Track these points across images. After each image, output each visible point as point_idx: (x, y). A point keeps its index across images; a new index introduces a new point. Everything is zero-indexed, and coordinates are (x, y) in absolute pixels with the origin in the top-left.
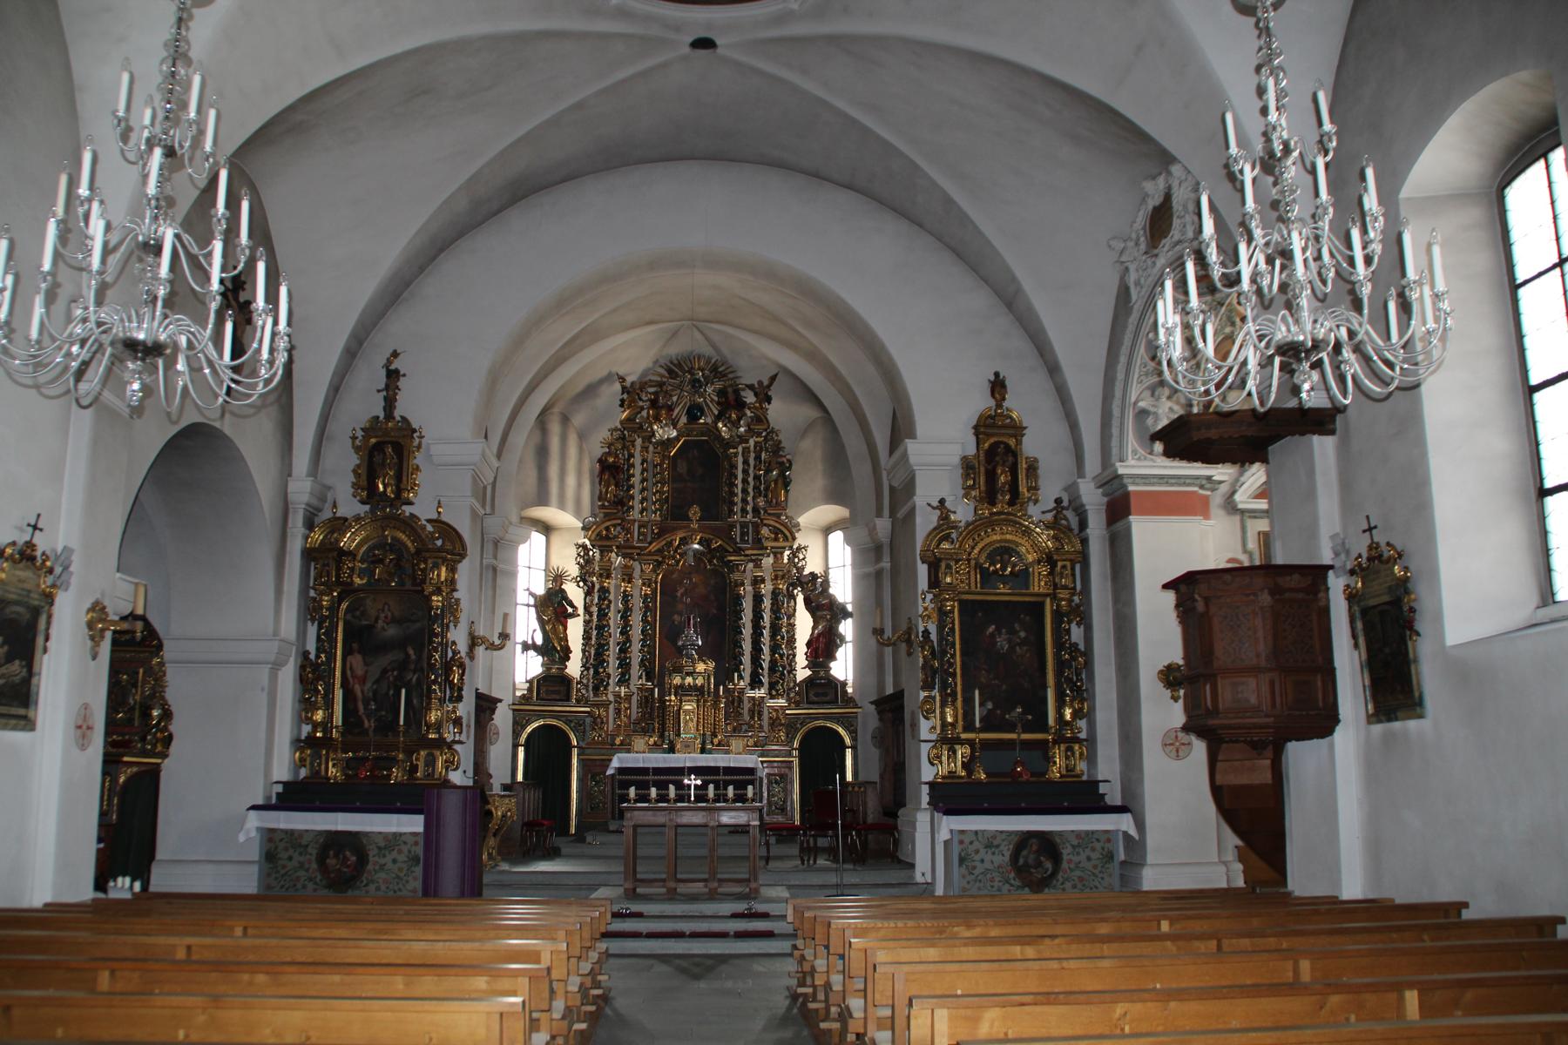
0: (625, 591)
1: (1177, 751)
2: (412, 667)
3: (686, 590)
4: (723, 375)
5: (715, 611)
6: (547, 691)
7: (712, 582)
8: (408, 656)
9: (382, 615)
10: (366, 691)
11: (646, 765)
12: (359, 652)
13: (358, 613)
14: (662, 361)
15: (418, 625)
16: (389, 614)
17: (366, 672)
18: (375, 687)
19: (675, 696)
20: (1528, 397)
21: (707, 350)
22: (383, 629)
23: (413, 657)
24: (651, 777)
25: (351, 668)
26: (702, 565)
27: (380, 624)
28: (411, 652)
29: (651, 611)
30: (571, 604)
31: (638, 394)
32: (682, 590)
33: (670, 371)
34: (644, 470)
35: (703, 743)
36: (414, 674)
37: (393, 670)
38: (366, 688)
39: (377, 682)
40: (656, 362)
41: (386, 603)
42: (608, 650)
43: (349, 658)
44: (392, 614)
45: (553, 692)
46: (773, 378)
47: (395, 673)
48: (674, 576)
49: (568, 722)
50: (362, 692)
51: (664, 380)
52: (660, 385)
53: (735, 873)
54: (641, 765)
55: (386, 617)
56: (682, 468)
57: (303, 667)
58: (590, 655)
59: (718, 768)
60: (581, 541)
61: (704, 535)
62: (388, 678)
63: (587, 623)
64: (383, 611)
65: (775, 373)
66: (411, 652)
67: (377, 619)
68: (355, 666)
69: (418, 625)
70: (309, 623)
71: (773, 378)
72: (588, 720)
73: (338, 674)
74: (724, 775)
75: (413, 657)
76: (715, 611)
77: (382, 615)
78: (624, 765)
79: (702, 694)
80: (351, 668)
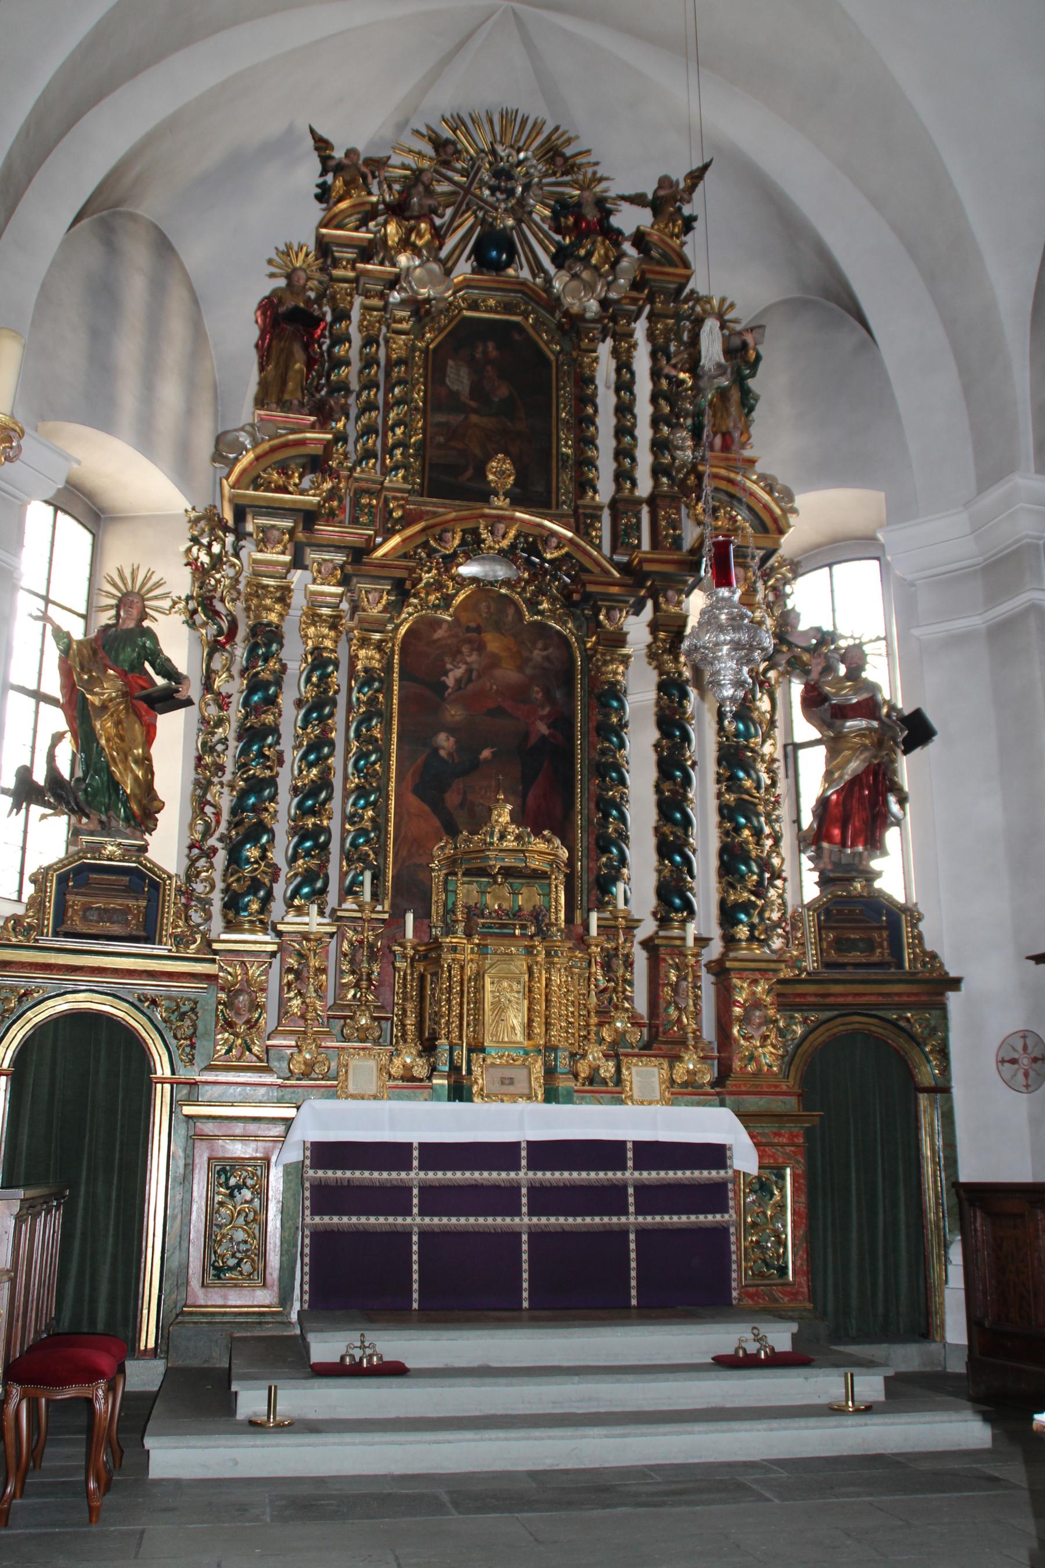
0: (317, 650)
1: (1013, 1061)
3: (469, 671)
4: (570, 167)
5: (543, 729)
6: (87, 908)
7: (537, 654)
19: (469, 935)
21: (534, 109)
24: (415, 1176)
26: (511, 611)
29: (379, 714)
30: (167, 670)
31: (364, 177)
32: (459, 672)
33: (439, 144)
34: (370, 384)
35: (550, 1072)
40: (401, 127)
42: (273, 799)
45: (106, 914)
46: (696, 177)
48: (440, 633)
49: (145, 1004)
51: (426, 164)
53: (222, 1104)
58: (218, 815)
59: (619, 1146)
60: (268, 272)
63: (208, 726)
65: (697, 164)
71: (696, 177)
72: (211, 998)
73: (854, 1188)
76: (543, 729)
79: (543, 933)
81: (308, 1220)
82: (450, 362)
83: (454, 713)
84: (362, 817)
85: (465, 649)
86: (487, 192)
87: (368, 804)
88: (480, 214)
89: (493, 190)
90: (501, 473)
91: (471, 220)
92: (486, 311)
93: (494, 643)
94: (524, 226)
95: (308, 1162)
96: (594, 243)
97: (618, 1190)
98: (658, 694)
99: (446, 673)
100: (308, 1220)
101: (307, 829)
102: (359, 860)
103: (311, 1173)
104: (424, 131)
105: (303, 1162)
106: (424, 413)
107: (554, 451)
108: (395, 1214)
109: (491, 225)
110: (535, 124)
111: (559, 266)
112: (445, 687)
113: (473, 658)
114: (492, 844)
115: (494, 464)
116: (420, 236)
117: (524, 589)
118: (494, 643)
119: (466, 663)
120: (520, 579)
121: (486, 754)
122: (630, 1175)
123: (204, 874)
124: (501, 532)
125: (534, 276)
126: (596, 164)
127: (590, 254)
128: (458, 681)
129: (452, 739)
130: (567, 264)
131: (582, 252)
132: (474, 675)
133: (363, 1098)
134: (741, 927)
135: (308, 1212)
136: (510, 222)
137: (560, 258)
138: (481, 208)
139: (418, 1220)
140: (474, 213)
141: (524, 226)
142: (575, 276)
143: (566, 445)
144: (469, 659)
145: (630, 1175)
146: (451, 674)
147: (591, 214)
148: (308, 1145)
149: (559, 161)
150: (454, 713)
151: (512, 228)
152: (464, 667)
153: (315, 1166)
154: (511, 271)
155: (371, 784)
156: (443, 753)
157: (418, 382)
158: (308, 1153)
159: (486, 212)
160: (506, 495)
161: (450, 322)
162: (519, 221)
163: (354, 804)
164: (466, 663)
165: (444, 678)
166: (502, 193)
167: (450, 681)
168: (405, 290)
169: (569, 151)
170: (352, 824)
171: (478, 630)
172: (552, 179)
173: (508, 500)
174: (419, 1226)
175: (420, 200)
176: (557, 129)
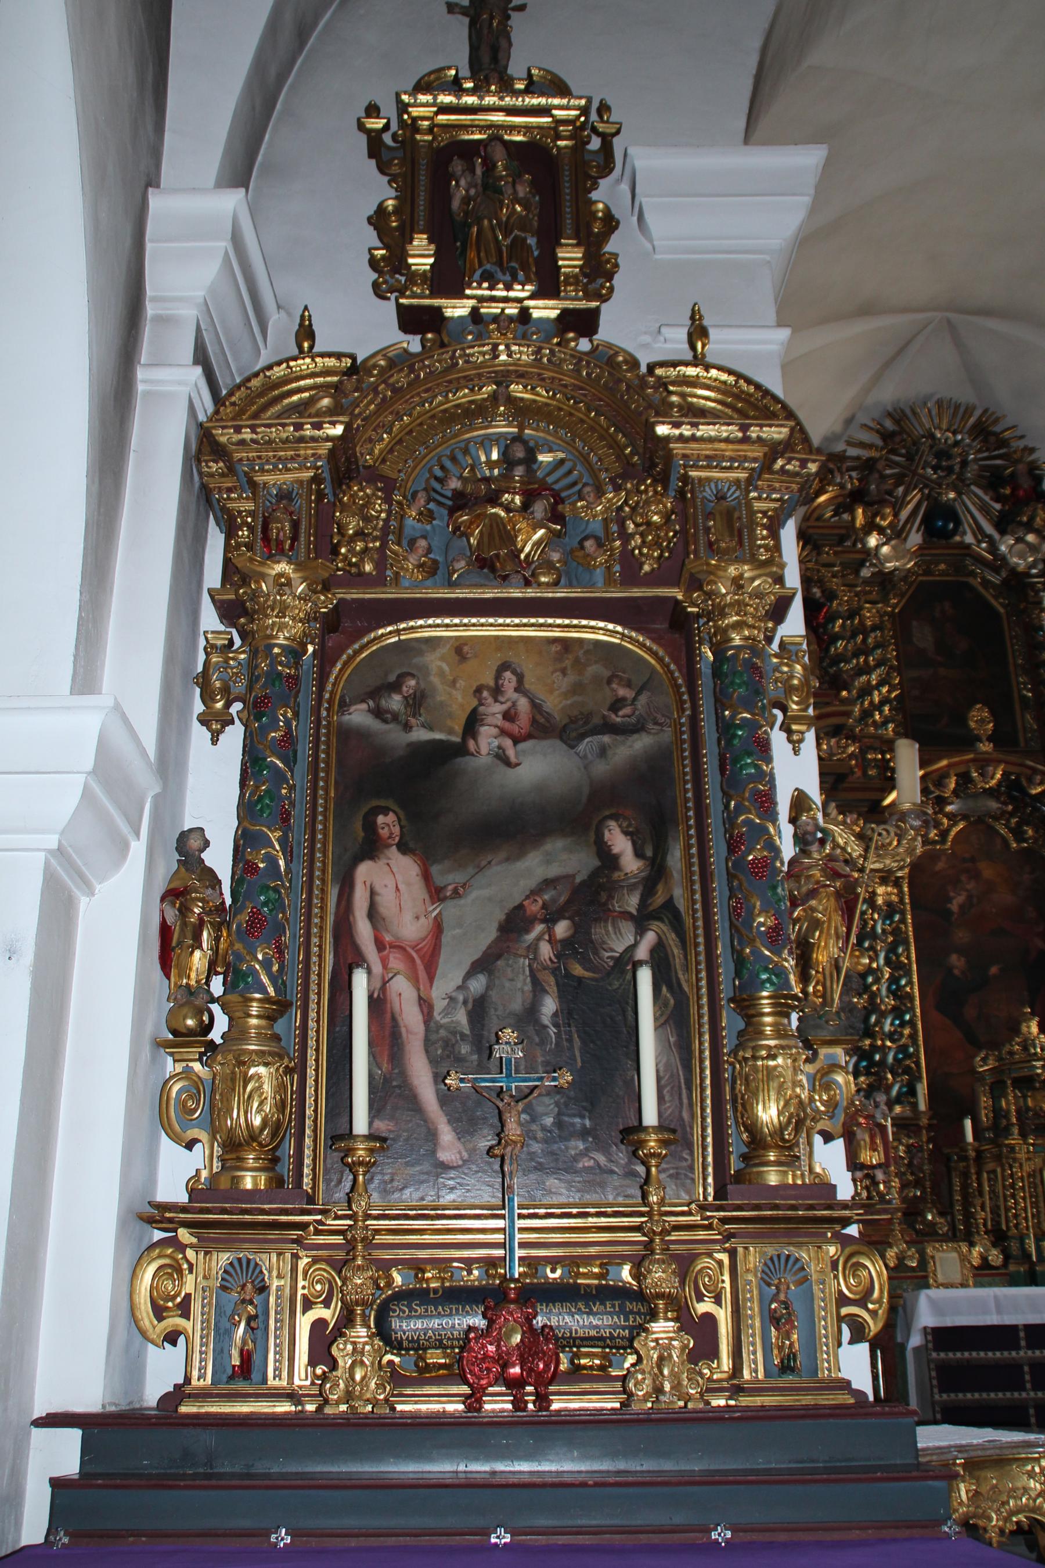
2: (632, 902)
3: (970, 897)
8: (609, 860)
9: (495, 710)
10: (440, 1005)
11: (1008, 1320)
12: (403, 848)
13: (395, 702)
14: (863, 418)
15: (640, 744)
16: (523, 704)
17: (438, 928)
18: (478, 984)
19: (1024, 1135)
20: (127, 1275)
21: (965, 395)
22: (501, 757)
23: (631, 864)
25: (373, 913)
27: (487, 739)
28: (620, 843)
36: (641, 931)
37: (550, 920)
38: (440, 991)
39: (483, 965)
40: (849, 421)
41: (504, 667)
43: (364, 871)
44: (536, 706)
47: (562, 929)
48: (940, 865)
50: (425, 1005)
51: (873, 454)
52: (867, 466)
54: (993, 1319)
55: (509, 716)
56: (923, 637)
57: (175, 895)
61: (1011, 768)
62: (534, 947)
64: (497, 691)
66: (620, 843)
67: (473, 723)
68: (387, 901)
69: (640, 744)
70: (199, 734)
74: (1030, 1346)
75: (631, 864)
77: (495, 710)
78: (949, 1322)
80: (373, 913)
81: (937, 1397)
82: (915, 623)
83: (962, 936)
84: (901, 1035)
85: (963, 878)
86: (930, 471)
87: (903, 1024)
88: (926, 491)
89: (935, 468)
90: (982, 722)
91: (919, 496)
92: (938, 575)
93: (987, 871)
94: (964, 497)
95: (930, 1345)
96: (1035, 510)
97: (1015, 1367)
98: (209, 729)
99: (950, 900)
100: (937, 1397)
101: (865, 1050)
102: (904, 1073)
103: (934, 1355)
104: (872, 425)
105: (926, 1345)
106: (899, 670)
107: (1016, 695)
108: (1012, 1389)
109: (936, 499)
110: (967, 409)
111: (1003, 532)
112: (950, 913)
113: (971, 886)
114: (1036, 1054)
115: (975, 713)
116: (883, 518)
117: (1008, 821)
118: (987, 871)
119: (967, 890)
120: (1004, 812)
121: (994, 970)
122: (1023, 1354)
123: (817, 1097)
124: (991, 773)
125: (979, 542)
126: (1022, 437)
127: (1032, 519)
128: (961, 907)
129: (963, 959)
130: (1009, 529)
131: (1025, 519)
132: (975, 900)
133: (952, 1287)
134: (469, 1050)
135: (936, 1390)
136: (952, 495)
137: (1003, 524)
138: (926, 486)
139: (1032, 1394)
140: (921, 490)
141: (964, 497)
142: (1019, 540)
143: (1025, 688)
144: (969, 887)
145: (1023, 1354)
146: (955, 902)
147: (1026, 483)
148: (929, 1331)
149: (992, 439)
150: (962, 936)
151: (954, 500)
152: (964, 894)
153: (937, 1349)
154: (958, 538)
155: (905, 1005)
156: (956, 972)
157: (891, 644)
158: (930, 1338)
159: (932, 489)
160: (990, 739)
161: (909, 587)
162: (959, 494)
163: (892, 1024)
164: (967, 890)
165: (949, 905)
166: (943, 471)
167: (954, 907)
168: (874, 565)
169: (997, 429)
170: (892, 1041)
171: (973, 860)
172: (985, 454)
173: (991, 745)
174: (1033, 1399)
175: (877, 486)
176: (986, 411)
